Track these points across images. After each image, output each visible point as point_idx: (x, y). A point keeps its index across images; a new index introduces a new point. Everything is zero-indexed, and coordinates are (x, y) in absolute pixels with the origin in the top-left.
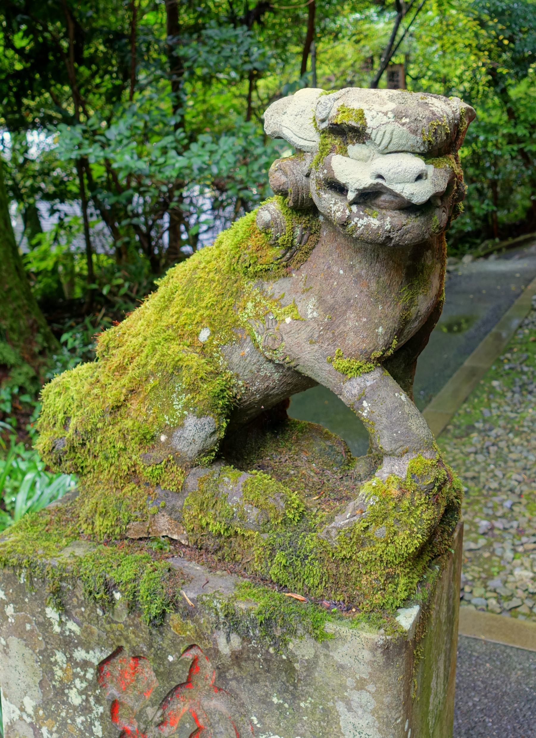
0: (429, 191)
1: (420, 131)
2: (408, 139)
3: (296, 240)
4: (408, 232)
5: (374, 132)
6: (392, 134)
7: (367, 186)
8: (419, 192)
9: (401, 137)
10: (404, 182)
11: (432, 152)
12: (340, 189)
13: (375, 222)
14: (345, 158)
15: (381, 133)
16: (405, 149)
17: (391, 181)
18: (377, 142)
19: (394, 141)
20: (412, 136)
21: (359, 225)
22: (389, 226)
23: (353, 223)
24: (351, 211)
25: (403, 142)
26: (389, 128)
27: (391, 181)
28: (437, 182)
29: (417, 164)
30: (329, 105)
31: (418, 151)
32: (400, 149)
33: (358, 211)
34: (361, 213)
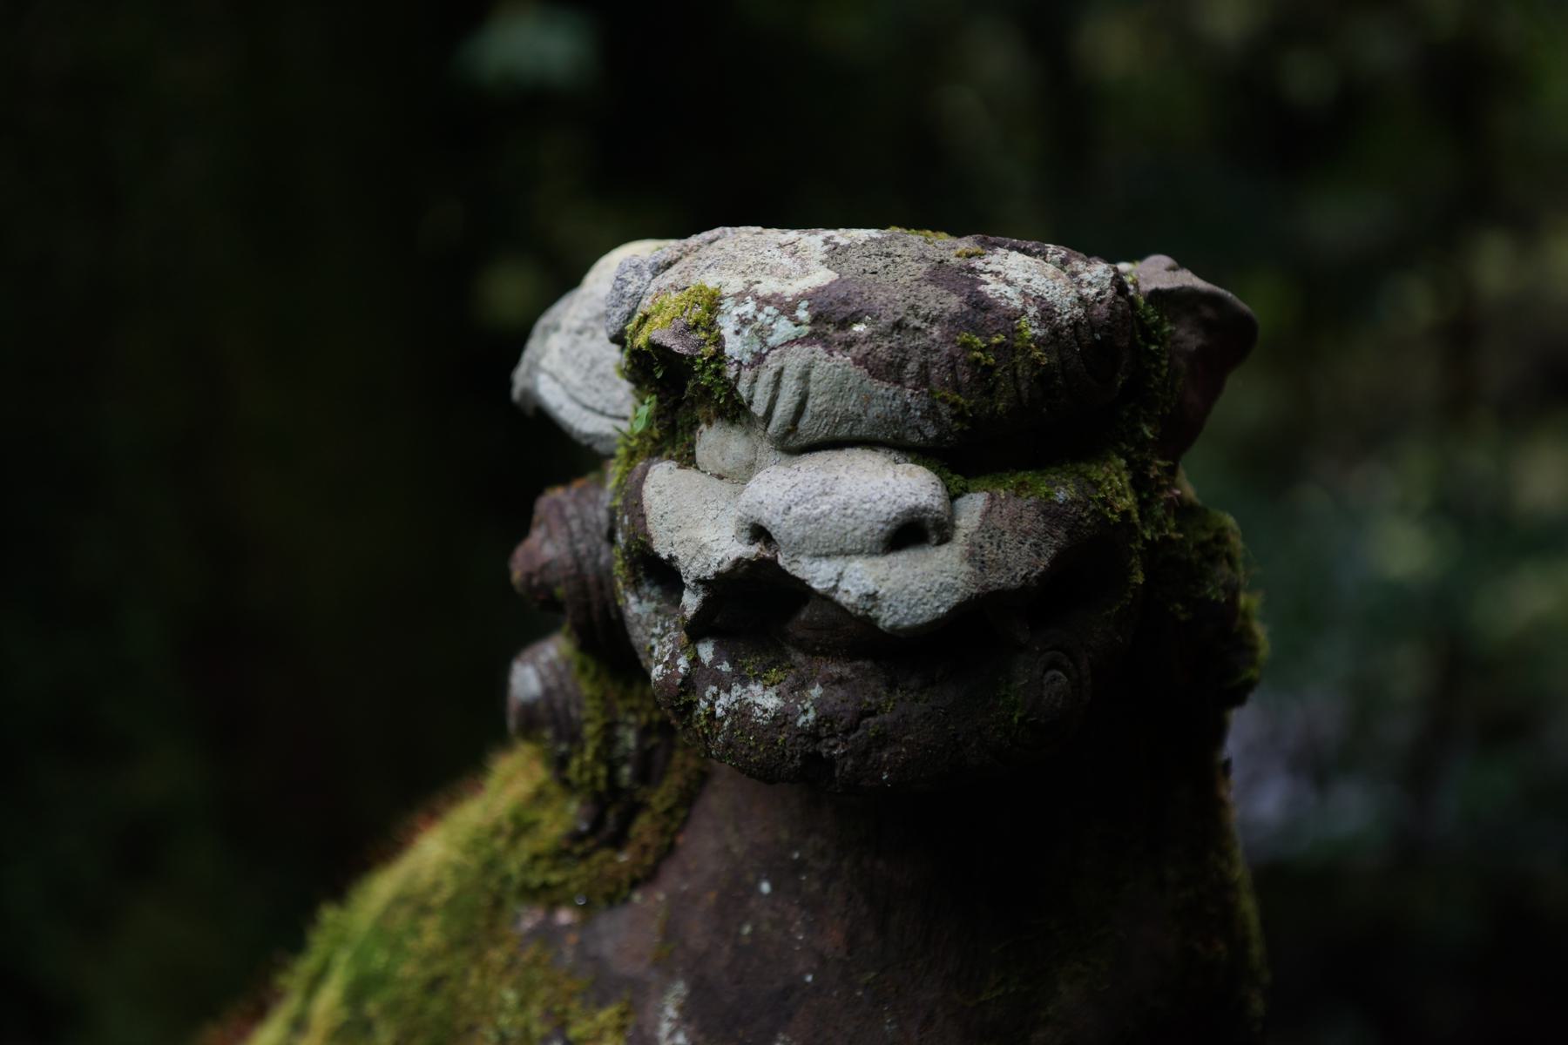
0: (945, 588)
1: (912, 367)
2: (868, 399)
3: (626, 771)
4: (882, 740)
5: (747, 374)
6: (805, 376)
7: (725, 567)
8: (914, 587)
9: (840, 390)
10: (844, 553)
11: (963, 444)
12: (661, 574)
13: (765, 700)
14: (690, 473)
15: (766, 376)
16: (862, 430)
17: (797, 549)
18: (759, 408)
19: (816, 404)
20: (882, 388)
21: (719, 712)
22: (811, 716)
23: (703, 704)
24: (695, 661)
25: (852, 404)
26: (796, 359)
27: (797, 549)
28: (990, 553)
29: (906, 485)
30: (631, 289)
31: (916, 439)
32: (843, 432)
33: (717, 660)
34: (725, 667)
